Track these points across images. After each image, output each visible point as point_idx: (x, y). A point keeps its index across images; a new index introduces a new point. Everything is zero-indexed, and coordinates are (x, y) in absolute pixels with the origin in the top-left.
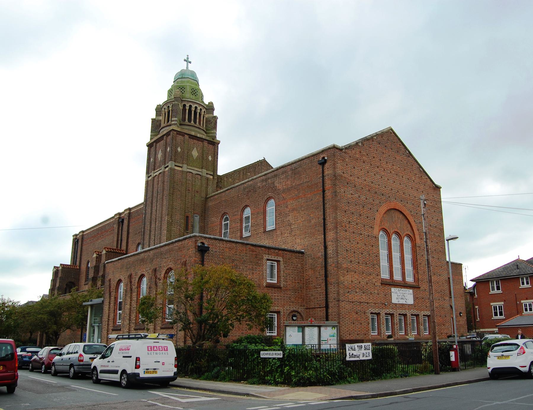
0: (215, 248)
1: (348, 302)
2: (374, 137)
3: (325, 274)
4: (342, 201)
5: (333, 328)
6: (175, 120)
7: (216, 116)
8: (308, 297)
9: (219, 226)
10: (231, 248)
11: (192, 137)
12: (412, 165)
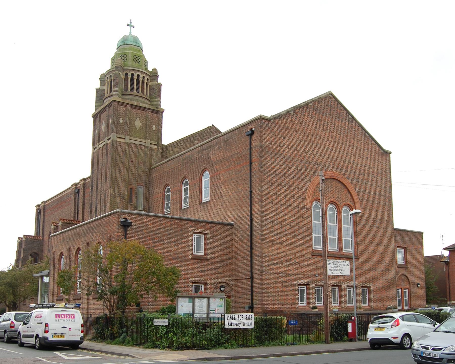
1: (273, 273)
2: (309, 104)
4: (269, 173)
5: (221, 299)
7: (160, 83)
9: (161, 198)
10: (155, 222)
11: (133, 106)
12: (356, 131)
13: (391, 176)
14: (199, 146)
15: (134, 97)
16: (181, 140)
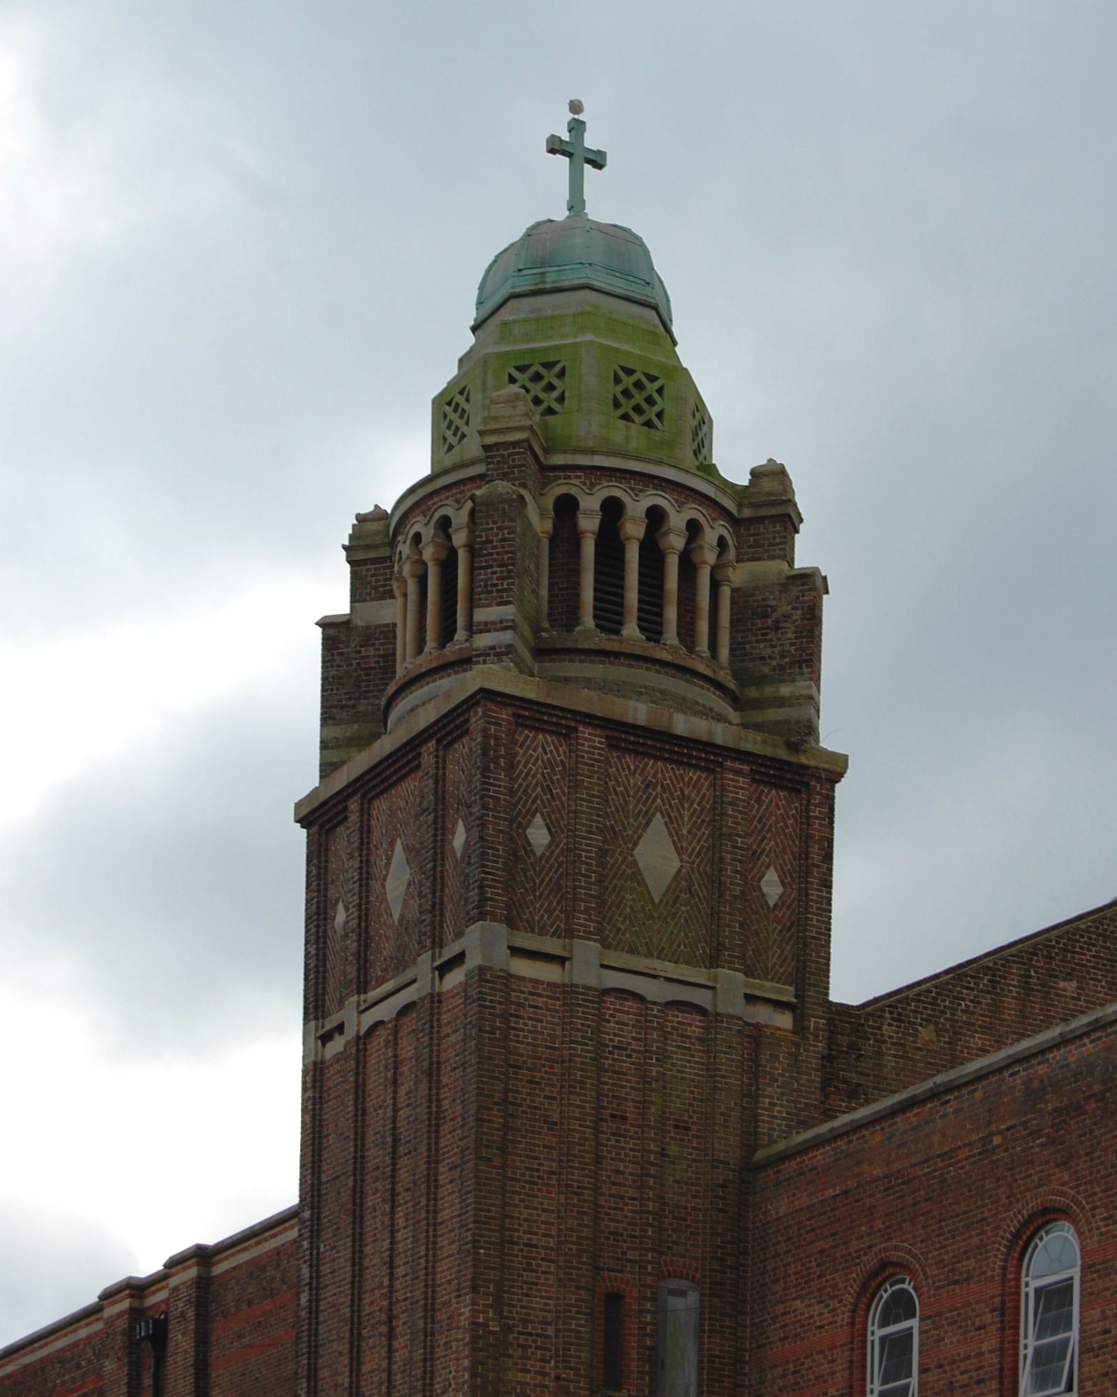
16: (959, 973)
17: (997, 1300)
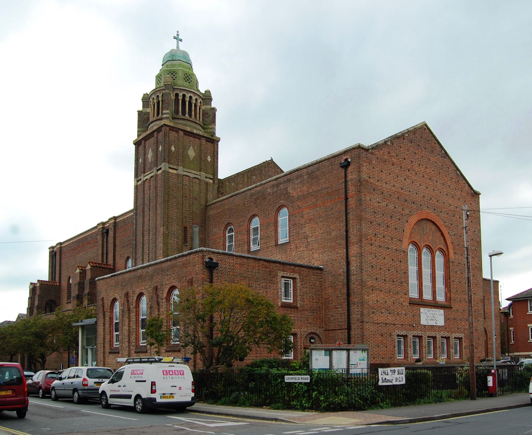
0: (224, 264)
2: (405, 135)
3: (347, 293)
5: (363, 352)
6: (167, 113)
8: (327, 318)
9: (222, 239)
11: (187, 133)
12: (449, 168)
13: (480, 219)
14: (274, 180)
15: (186, 122)
16: (238, 174)
17: (247, 230)
